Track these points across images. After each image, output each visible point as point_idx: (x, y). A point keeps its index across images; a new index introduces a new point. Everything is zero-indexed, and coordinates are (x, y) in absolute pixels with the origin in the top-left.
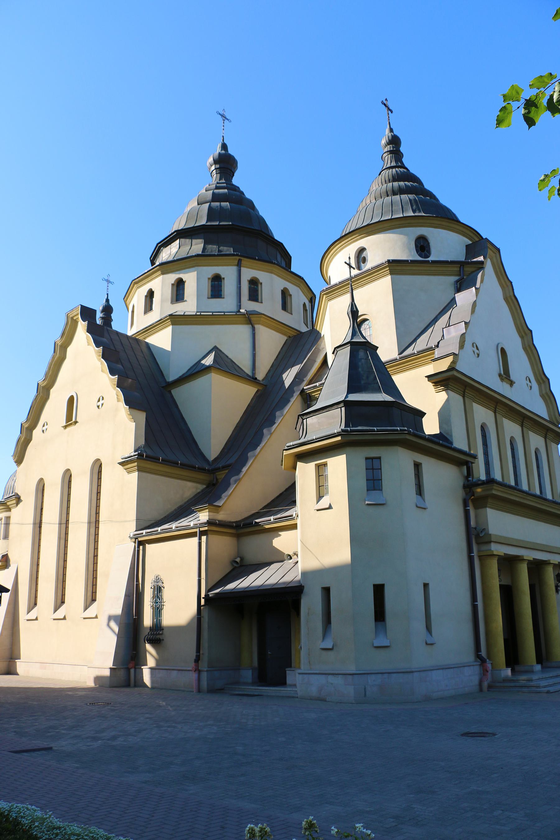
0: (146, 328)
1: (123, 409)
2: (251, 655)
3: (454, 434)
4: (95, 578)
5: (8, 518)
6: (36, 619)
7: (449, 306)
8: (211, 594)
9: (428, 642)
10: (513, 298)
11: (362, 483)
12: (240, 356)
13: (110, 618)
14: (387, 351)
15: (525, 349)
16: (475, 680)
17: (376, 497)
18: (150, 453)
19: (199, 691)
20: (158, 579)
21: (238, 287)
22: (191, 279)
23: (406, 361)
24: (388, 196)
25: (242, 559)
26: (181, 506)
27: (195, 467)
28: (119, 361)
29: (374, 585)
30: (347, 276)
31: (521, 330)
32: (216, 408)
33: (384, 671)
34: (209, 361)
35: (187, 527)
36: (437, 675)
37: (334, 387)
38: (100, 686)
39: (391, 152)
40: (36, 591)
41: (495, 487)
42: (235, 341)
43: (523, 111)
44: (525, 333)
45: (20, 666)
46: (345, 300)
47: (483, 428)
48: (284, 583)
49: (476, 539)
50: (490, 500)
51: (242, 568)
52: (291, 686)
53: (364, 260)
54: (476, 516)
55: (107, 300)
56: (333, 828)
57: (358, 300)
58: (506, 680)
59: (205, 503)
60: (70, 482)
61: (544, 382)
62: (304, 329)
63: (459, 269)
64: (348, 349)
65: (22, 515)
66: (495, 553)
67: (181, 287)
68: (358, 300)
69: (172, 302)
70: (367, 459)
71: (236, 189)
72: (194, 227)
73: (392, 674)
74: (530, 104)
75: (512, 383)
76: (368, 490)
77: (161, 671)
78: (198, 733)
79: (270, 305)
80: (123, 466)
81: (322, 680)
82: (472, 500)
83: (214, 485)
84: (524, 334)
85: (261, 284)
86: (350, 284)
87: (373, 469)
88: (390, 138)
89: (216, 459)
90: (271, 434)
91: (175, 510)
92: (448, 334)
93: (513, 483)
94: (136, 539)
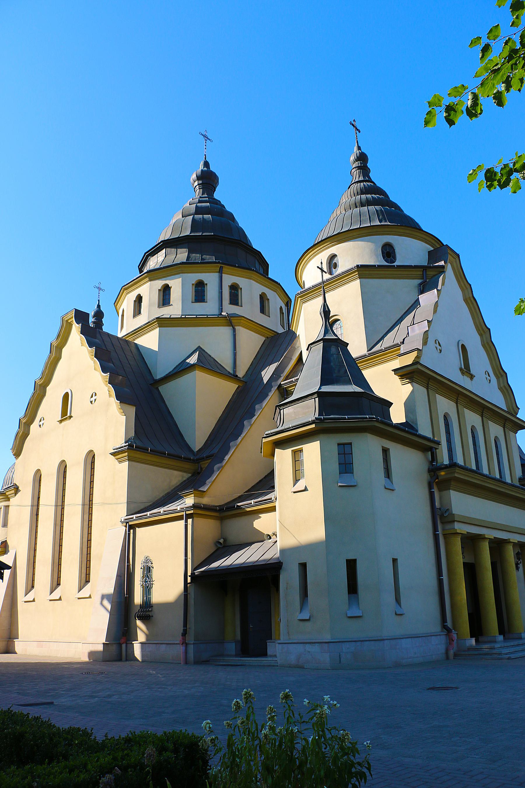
0: (135, 330)
1: (114, 403)
2: (234, 630)
4: (89, 561)
5: (7, 507)
6: (34, 601)
7: (413, 306)
8: (197, 572)
9: (398, 613)
10: (472, 299)
11: (335, 466)
12: (222, 354)
13: (103, 597)
14: (357, 347)
15: (484, 346)
16: (442, 648)
17: (347, 479)
18: (140, 444)
19: (186, 663)
20: (147, 560)
21: (219, 292)
22: (176, 284)
23: (374, 356)
24: (356, 207)
25: (225, 540)
26: (168, 493)
27: (181, 457)
28: (110, 360)
29: (347, 561)
30: (320, 280)
31: (480, 329)
32: (201, 403)
34: (193, 360)
35: (175, 511)
36: (405, 643)
37: (309, 380)
38: (94, 661)
39: (359, 168)
40: (34, 574)
41: (457, 471)
42: (217, 342)
43: (445, 114)
44: (484, 331)
45: (19, 646)
46: (319, 301)
47: (446, 417)
48: (264, 560)
49: (441, 519)
50: (453, 483)
51: (225, 548)
52: (271, 656)
53: (335, 266)
54: (441, 498)
55: (99, 306)
56: (305, 700)
57: (331, 302)
58: (471, 649)
59: (191, 488)
60: (65, 472)
61: (502, 376)
62: (281, 330)
63: (421, 273)
64: (321, 345)
65: (20, 506)
67: (167, 292)
68: (331, 302)
69: (159, 307)
70: (339, 444)
71: (217, 202)
72: (179, 237)
74: (450, 109)
75: (472, 377)
77: (151, 645)
78: (187, 692)
79: (249, 308)
80: (114, 456)
81: (300, 648)
82: (436, 483)
83: (199, 473)
84: (482, 332)
85: (241, 289)
86: (322, 288)
87: (345, 454)
88: (358, 155)
89: (200, 450)
90: (251, 425)
91: (163, 497)
92: (412, 332)
93: (474, 467)
94: (127, 523)
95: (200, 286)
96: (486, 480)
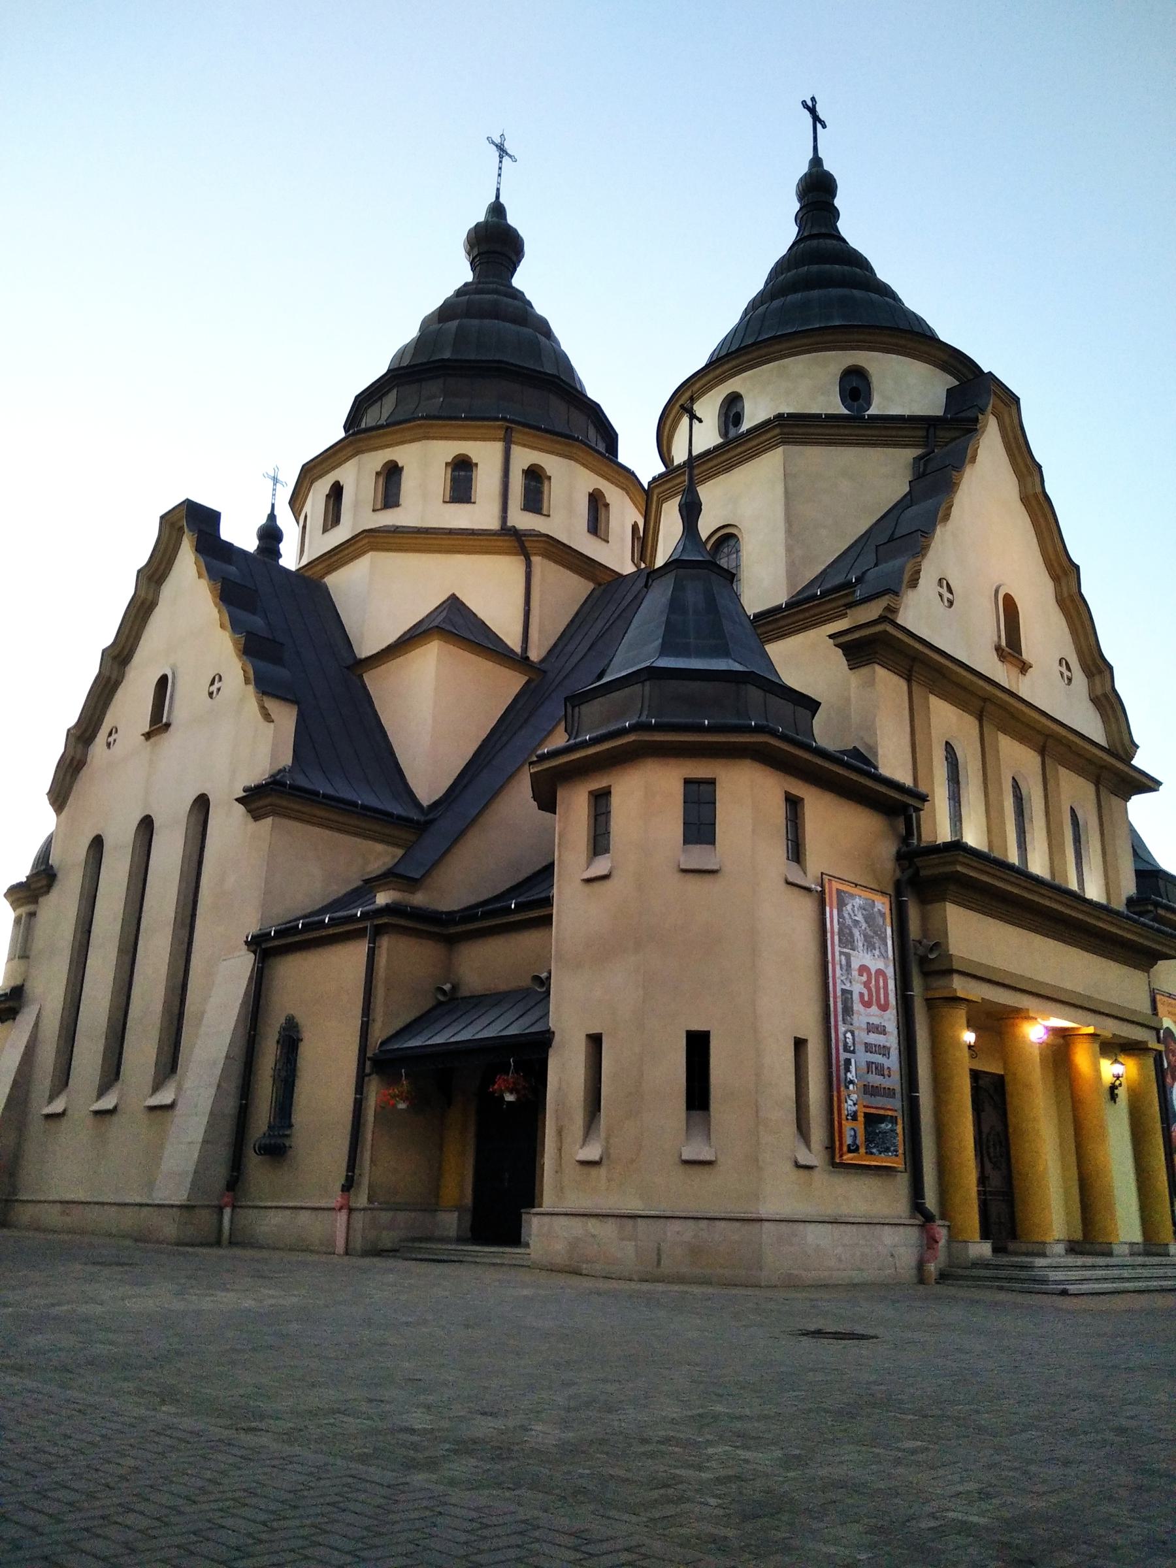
2: (459, 1181)
3: (880, 752)
10: (1041, 498)
16: (907, 1257)
17: (698, 857)
33: (699, 1215)
36: (814, 1235)
44: (1063, 571)
53: (738, 419)
54: (924, 919)
66: (960, 994)
70: (687, 782)
73: (717, 1223)
76: (686, 841)
81: (577, 1227)
85: (550, 478)
95: (462, 468)
96: (1035, 889)
